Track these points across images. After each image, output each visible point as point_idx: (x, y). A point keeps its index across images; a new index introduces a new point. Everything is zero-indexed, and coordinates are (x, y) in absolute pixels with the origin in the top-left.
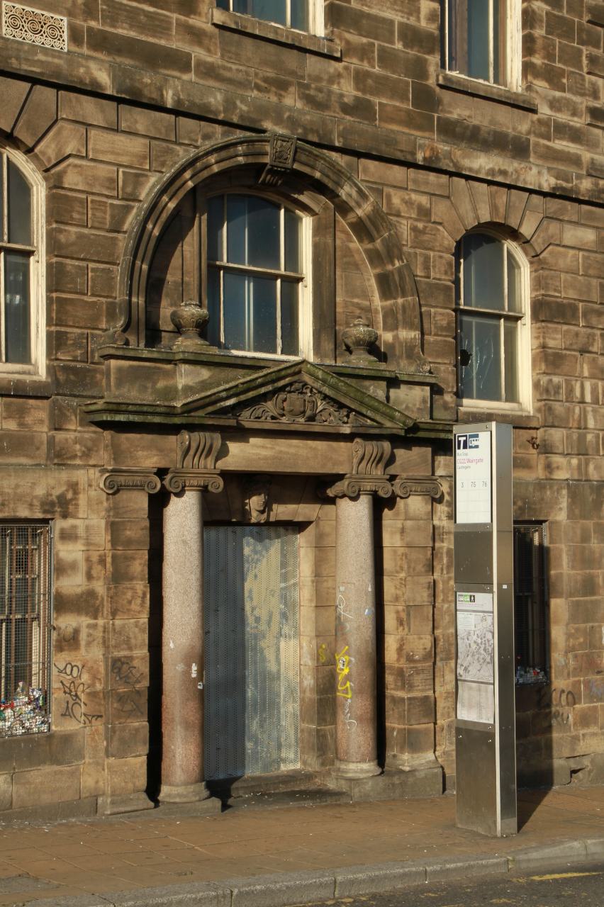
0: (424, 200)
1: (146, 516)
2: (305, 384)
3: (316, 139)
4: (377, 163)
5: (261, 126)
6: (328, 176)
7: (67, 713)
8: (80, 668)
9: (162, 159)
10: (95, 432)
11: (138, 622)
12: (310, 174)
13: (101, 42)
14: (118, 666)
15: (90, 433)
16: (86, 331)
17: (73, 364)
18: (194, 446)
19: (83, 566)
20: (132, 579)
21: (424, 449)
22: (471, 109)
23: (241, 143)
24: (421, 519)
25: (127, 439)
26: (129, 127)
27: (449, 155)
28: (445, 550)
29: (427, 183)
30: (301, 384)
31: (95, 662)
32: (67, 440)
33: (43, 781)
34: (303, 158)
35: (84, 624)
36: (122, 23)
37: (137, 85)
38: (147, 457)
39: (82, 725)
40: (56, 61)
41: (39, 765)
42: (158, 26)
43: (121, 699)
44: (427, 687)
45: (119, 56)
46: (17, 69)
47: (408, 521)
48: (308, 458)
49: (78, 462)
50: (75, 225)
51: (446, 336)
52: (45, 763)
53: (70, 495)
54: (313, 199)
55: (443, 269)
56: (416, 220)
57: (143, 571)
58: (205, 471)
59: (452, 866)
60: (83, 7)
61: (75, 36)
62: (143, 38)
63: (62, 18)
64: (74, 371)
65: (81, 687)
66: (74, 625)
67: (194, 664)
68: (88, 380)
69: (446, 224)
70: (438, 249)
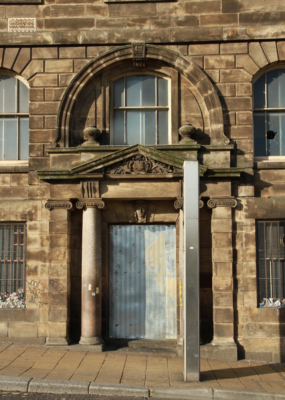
0: (231, 58)
1: (66, 219)
2: (142, 156)
3: (159, 41)
4: (199, 45)
5: (128, 41)
6: (166, 57)
7: (32, 301)
8: (38, 282)
9: (79, 66)
10: (47, 185)
11: (62, 264)
12: (156, 58)
13: (50, 24)
14: (53, 283)
15: (45, 185)
16: (43, 144)
17: (37, 157)
18: (85, 187)
19: (39, 241)
20: (59, 246)
21: (225, 183)
22: (264, 5)
23: (116, 51)
24: (224, 218)
25: (57, 187)
26: (63, 56)
27: (245, 32)
28: (244, 234)
29: (232, 49)
30: (140, 156)
31: (45, 280)
32: (34, 189)
33: (21, 329)
34: (151, 51)
35: (40, 265)
36: (61, 13)
37: (65, 38)
38: (66, 194)
39: (38, 306)
40: (28, 36)
41: (19, 321)
42: (77, 11)
43: (54, 297)
44: (229, 304)
45: (59, 28)
46: (11, 43)
47: (215, 220)
48: (153, 191)
49: (39, 198)
50: (39, 101)
51: (246, 125)
52: (22, 320)
53: (33, 211)
54: (166, 70)
55: (244, 91)
56: (225, 69)
57: (64, 243)
58: (94, 199)
59: (107, 388)
60: (43, 12)
61: (39, 25)
62: (71, 17)
63: (33, 19)
64: (38, 160)
65: (38, 290)
66: (35, 264)
67: (90, 284)
68: (43, 164)
69: (245, 67)
70: (241, 81)
